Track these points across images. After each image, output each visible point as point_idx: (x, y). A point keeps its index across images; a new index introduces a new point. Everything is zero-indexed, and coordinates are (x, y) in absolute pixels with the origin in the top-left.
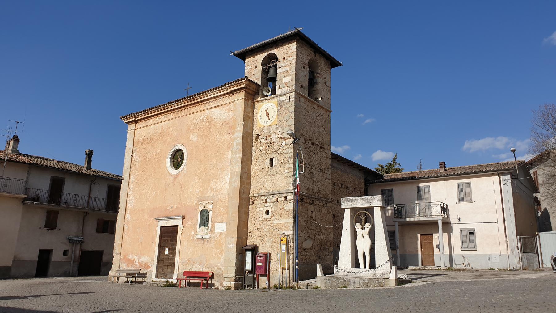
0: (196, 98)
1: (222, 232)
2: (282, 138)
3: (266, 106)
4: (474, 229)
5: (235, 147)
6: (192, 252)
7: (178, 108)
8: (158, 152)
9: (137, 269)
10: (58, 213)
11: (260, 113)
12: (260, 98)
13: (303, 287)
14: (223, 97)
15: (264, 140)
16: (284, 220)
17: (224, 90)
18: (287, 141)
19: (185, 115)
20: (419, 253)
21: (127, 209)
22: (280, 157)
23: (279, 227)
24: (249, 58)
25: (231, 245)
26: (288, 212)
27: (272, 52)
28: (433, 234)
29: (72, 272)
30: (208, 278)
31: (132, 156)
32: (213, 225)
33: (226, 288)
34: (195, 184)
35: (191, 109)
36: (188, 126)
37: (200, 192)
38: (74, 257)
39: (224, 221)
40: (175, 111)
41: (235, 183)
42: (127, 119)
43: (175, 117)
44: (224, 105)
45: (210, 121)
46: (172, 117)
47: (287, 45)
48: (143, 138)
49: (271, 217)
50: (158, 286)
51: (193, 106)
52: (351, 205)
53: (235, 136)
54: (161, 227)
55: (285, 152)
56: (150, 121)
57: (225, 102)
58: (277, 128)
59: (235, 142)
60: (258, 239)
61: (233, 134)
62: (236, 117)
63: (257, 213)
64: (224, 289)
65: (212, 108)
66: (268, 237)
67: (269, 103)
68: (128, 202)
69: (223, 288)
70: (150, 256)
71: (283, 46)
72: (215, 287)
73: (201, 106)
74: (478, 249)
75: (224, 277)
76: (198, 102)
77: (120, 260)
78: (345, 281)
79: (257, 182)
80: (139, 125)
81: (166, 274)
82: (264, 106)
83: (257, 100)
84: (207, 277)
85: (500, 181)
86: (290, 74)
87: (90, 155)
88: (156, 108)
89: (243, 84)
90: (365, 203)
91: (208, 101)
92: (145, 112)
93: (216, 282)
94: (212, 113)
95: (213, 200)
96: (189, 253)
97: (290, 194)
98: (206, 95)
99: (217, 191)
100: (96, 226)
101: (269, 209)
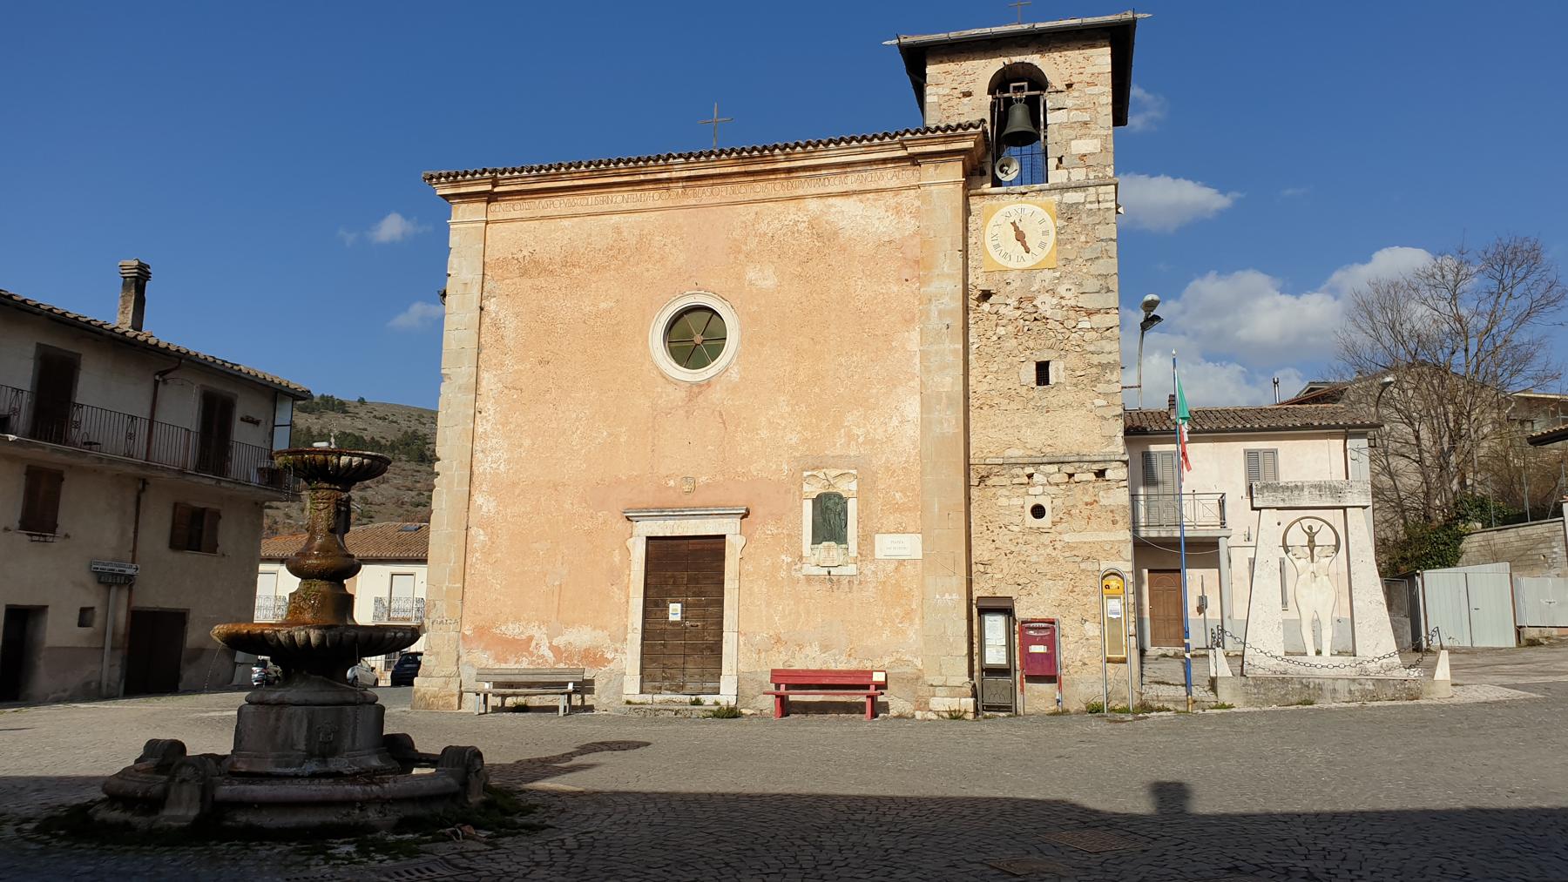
0: (773, 156)
2: (1077, 309)
6: (790, 614)
8: (603, 305)
10: (63, 480)
11: (990, 230)
12: (989, 185)
13: (1177, 705)
14: (875, 167)
15: (1011, 308)
16: (1102, 534)
22: (1073, 359)
23: (1084, 552)
24: (941, 62)
26: (1112, 511)
27: (1027, 61)
29: (108, 685)
30: (872, 687)
32: (866, 539)
33: (946, 715)
34: (782, 417)
36: (735, 240)
37: (805, 441)
38: (114, 634)
40: (671, 185)
41: (946, 425)
42: (455, 183)
44: (877, 191)
45: (825, 237)
46: (659, 204)
47: (1079, 49)
49: (1054, 524)
50: (679, 716)
51: (752, 179)
52: (1283, 500)
53: (932, 289)
55: (1092, 348)
56: (558, 204)
58: (1058, 279)
59: (933, 307)
61: (923, 281)
62: (932, 232)
64: (934, 717)
65: (830, 195)
67: (1024, 206)
70: (603, 628)
72: (893, 712)
75: (932, 685)
78: (1308, 687)
80: (500, 210)
82: (1005, 209)
83: (979, 191)
85: (1345, 451)
86: (1095, 133)
87: (139, 281)
88: (598, 167)
89: (965, 141)
90: (1323, 496)
91: (814, 171)
94: (833, 210)
96: (777, 618)
98: (816, 154)
99: (873, 442)
100: (169, 526)
101: (1045, 502)
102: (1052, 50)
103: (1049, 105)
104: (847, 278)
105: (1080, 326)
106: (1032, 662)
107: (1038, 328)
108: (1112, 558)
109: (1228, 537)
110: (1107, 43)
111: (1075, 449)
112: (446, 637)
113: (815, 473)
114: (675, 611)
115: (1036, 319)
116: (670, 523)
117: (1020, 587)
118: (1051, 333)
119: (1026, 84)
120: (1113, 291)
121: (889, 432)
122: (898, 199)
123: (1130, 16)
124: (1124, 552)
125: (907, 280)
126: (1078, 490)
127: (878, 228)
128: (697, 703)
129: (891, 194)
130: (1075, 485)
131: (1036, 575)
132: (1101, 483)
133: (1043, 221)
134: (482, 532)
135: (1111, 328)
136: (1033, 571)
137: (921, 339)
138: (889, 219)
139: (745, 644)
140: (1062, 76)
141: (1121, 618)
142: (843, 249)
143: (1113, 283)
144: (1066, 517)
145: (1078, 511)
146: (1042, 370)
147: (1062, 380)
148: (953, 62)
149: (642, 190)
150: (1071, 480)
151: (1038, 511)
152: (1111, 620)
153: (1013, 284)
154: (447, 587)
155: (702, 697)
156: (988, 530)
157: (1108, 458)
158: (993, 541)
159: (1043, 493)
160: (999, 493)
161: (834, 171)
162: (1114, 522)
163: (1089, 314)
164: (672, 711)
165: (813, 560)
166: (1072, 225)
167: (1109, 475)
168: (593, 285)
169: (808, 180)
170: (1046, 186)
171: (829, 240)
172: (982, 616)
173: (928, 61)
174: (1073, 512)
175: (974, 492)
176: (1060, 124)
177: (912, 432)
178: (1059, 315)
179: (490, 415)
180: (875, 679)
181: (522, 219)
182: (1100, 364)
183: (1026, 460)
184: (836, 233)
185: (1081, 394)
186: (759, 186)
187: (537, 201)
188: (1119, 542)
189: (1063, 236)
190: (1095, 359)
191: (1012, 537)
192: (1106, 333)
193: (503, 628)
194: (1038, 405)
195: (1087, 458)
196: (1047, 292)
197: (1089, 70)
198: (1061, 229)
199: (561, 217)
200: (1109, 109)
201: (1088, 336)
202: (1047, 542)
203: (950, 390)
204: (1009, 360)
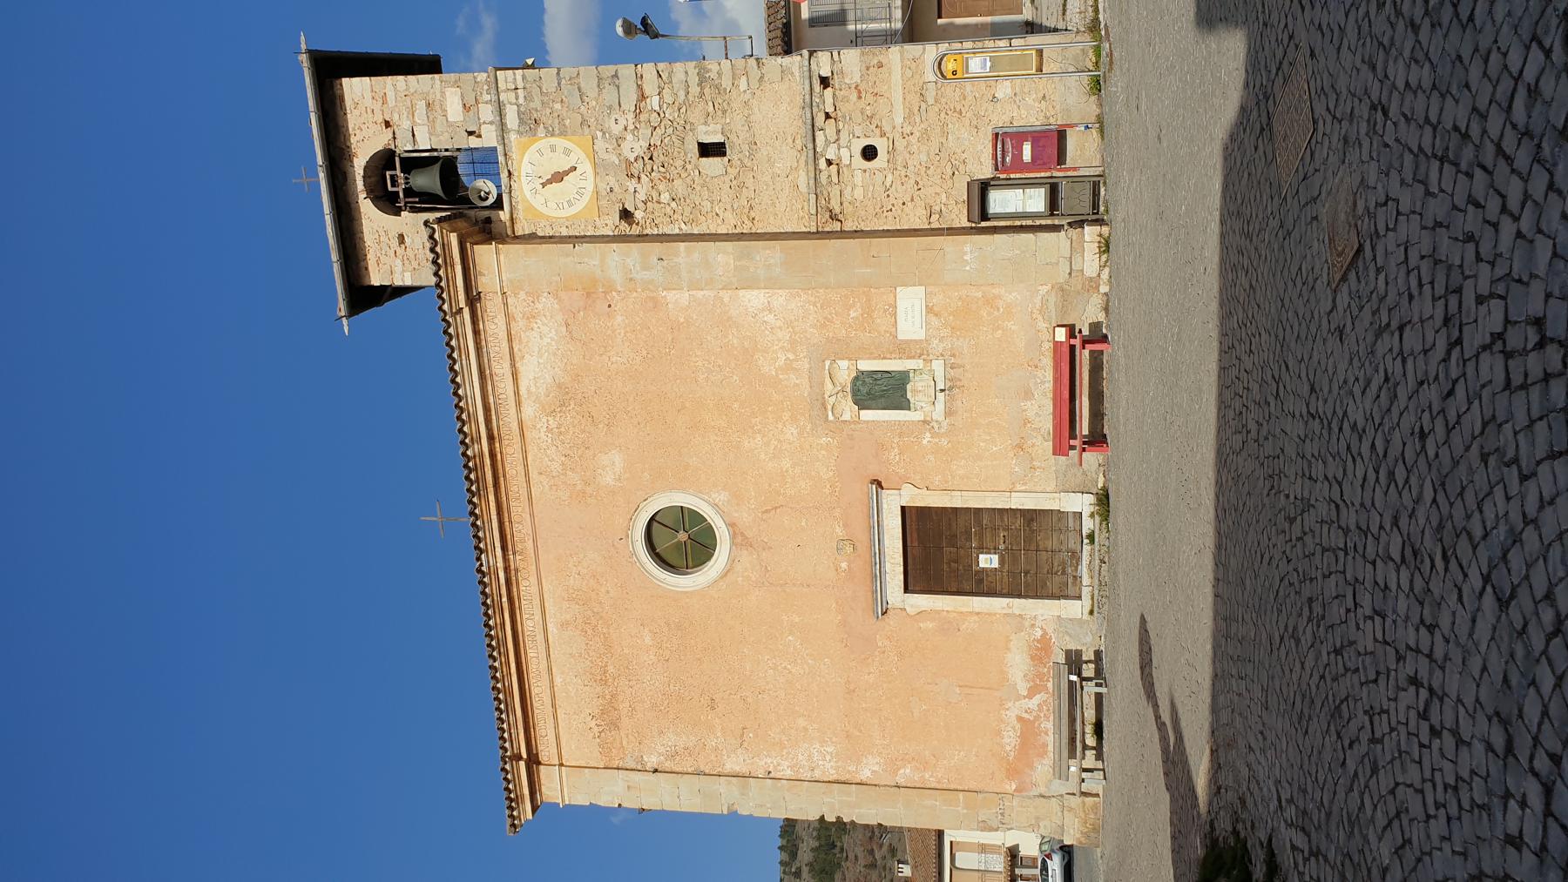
0: (475, 456)
1: (927, 306)
2: (638, 112)
3: (532, 185)
6: (990, 434)
7: (504, 548)
8: (648, 641)
9: (1051, 700)
14: (483, 343)
15: (639, 186)
17: (460, 330)
18: (647, 92)
19: (532, 515)
20: (989, 19)
21: (843, 779)
22: (695, 115)
23: (915, 100)
24: (367, 269)
25: (967, 257)
26: (868, 69)
27: (362, 173)
30: (1073, 342)
31: (656, 771)
32: (904, 349)
33: (1104, 257)
35: (513, 489)
40: (512, 567)
41: (772, 261)
42: (518, 799)
43: (534, 567)
44: (510, 340)
45: (563, 398)
46: (533, 579)
47: (345, 114)
48: (593, 724)
49: (883, 135)
50: (1106, 560)
53: (617, 277)
54: (905, 592)
55: (682, 94)
57: (503, 335)
58: (604, 133)
60: (950, 183)
63: (870, 195)
64: (1107, 270)
65: (517, 393)
66: (944, 141)
67: (523, 173)
68: (817, 775)
69: (1105, 274)
70: (1008, 640)
71: (348, 129)
72: (1101, 317)
73: (505, 442)
75: (1070, 274)
76: (492, 455)
77: (1024, 794)
79: (774, 204)
80: (546, 752)
81: (1065, 556)
82: (528, 194)
84: (1072, 348)
88: (494, 647)
89: (449, 244)
91: (490, 411)
92: (501, 706)
93: (1089, 314)
94: (533, 389)
95: (824, 361)
96: (995, 449)
97: (814, 66)
102: (348, 144)
104: (609, 373)
105: (657, 108)
110: (338, 82)
111: (797, 111)
112: (1020, 809)
113: (829, 407)
114: (988, 561)
115: (651, 158)
116: (888, 567)
117: (956, 173)
122: (519, 317)
123: (304, 58)
125: (610, 306)
126: (844, 108)
127: (552, 339)
128: (1091, 537)
129: (513, 324)
130: (838, 111)
132: (836, 82)
134: (902, 771)
135: (658, 72)
137: (674, 289)
139: (1025, 484)
144: (875, 122)
147: (719, 127)
149: (519, 598)
151: (869, 153)
153: (611, 184)
154: (963, 809)
155: (1085, 532)
156: (891, 210)
157: (807, 74)
158: (904, 204)
159: (849, 147)
161: (490, 388)
162: (880, 65)
164: (1101, 566)
165: (928, 408)
166: (544, 119)
167: (825, 73)
168: (626, 651)
170: (500, 149)
172: (989, 216)
173: (367, 283)
174: (869, 113)
175: (849, 226)
176: (430, 134)
179: (771, 763)
181: (556, 727)
182: (700, 84)
183: (811, 168)
184: (559, 386)
185: (734, 105)
186: (510, 472)
187: (536, 711)
188: (902, 60)
190: (695, 90)
191: (899, 183)
193: (1008, 748)
194: (747, 154)
195: (808, 97)
196: (619, 146)
197: (368, 102)
198: (548, 131)
199: (552, 687)
200: (411, 78)
201: (668, 98)
202: (904, 142)
204: (698, 188)
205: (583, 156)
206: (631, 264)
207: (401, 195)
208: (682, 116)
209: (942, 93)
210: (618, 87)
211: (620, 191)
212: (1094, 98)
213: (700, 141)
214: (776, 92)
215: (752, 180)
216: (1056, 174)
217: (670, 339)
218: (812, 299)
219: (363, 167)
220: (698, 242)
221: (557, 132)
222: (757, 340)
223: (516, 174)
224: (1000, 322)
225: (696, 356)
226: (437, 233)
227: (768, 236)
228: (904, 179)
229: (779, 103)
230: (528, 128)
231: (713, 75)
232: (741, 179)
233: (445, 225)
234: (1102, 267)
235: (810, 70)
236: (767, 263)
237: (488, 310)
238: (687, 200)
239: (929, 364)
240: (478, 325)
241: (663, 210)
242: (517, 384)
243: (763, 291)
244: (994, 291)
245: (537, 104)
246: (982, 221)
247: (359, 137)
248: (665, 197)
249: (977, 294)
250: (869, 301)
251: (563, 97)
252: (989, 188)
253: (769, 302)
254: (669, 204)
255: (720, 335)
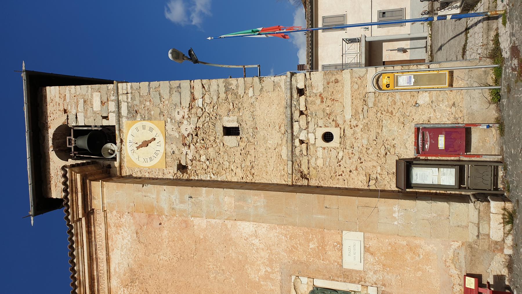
1: (365, 247)
2: (191, 107)
3: (132, 148)
4: (379, 12)
5: (187, 206)
14: (93, 239)
16: (345, 90)
18: (196, 96)
22: (222, 111)
23: (359, 104)
24: (50, 189)
25: (396, 215)
26: (328, 83)
28: (383, 61)
39: (339, 239)
41: (259, 204)
44: (107, 238)
47: (47, 105)
49: (337, 126)
53: (165, 207)
55: (215, 98)
58: (172, 120)
60: (383, 160)
63: (327, 164)
67: (128, 141)
69: (509, 240)
72: (505, 272)
74: (403, 7)
75: (478, 236)
79: (266, 166)
83: (118, 169)
86: (90, 96)
89: (76, 180)
91: (94, 280)
94: (117, 270)
95: (291, 276)
97: (294, 82)
99: (271, 261)
102: (47, 121)
103: (74, 124)
104: (158, 266)
105: (201, 106)
106: (453, 147)
107: (202, 134)
108: (364, 83)
109: (366, 37)
110: (44, 88)
111: (282, 109)
117: (388, 153)
118: (205, 125)
119: (68, 138)
120: (180, 84)
121: (264, 247)
122: (112, 225)
123: (24, 75)
124: (360, 74)
125: (160, 224)
126: (312, 108)
127: (129, 241)
130: (308, 110)
131: (378, 140)
132: (307, 93)
133: (137, 129)
135: (203, 85)
136: (375, 143)
137: (198, 217)
138: (123, 232)
140: (60, 116)
141: (414, 75)
142: (141, 266)
143: (175, 83)
144: (332, 117)
145: (327, 108)
146: (230, 131)
147: (236, 118)
148: (50, 181)
150: (305, 113)
151: (328, 137)
152: (416, 83)
153: (174, 149)
156: (341, 175)
157: (289, 87)
158: (350, 171)
159: (314, 133)
160: (314, 165)
162: (337, 81)
163: (194, 99)
166: (140, 110)
167: (301, 86)
169: (100, 284)
170: (117, 127)
171: (135, 275)
172: (412, 186)
174: (328, 112)
175: (313, 183)
176: (85, 117)
177: (263, 229)
178: (194, 119)
180: (473, 287)
182: (226, 92)
183: (290, 145)
184: (131, 270)
185: (245, 105)
188: (352, 77)
189: (146, 116)
190: (223, 96)
191: (347, 158)
192: (206, 88)
194: (252, 135)
195: (289, 101)
196: (180, 127)
197: (57, 99)
198: (142, 118)
200: (78, 87)
201: (208, 100)
202: (352, 131)
203: (233, 199)
204: (222, 153)
205: (159, 132)
206: (174, 199)
207: (73, 150)
208: (215, 111)
209: (379, 100)
210: (180, 93)
211: (178, 153)
212: (93, 208)
213: (225, 126)
214: (270, 98)
215: (254, 150)
216: (463, 158)
217: (194, 248)
218: (284, 232)
219: (53, 134)
220: (213, 188)
221: (147, 118)
222: (248, 255)
223: (124, 140)
224: (420, 265)
225: (210, 262)
226: (68, 174)
227: (260, 187)
228: (351, 155)
229: (271, 104)
230: (132, 116)
231: (233, 87)
232: (247, 149)
233: (76, 169)
234: (506, 234)
235: (291, 84)
236: (255, 205)
237: (97, 220)
238: (216, 161)
239: (366, 289)
240: (91, 228)
241: (202, 165)
242: (109, 265)
243: (252, 223)
244: (416, 242)
245: (137, 102)
246: (407, 188)
247: (52, 118)
248: (203, 158)
249: (402, 242)
250: (323, 238)
251: (151, 98)
252: (412, 166)
253: (256, 231)
254: (205, 163)
255: (224, 250)
